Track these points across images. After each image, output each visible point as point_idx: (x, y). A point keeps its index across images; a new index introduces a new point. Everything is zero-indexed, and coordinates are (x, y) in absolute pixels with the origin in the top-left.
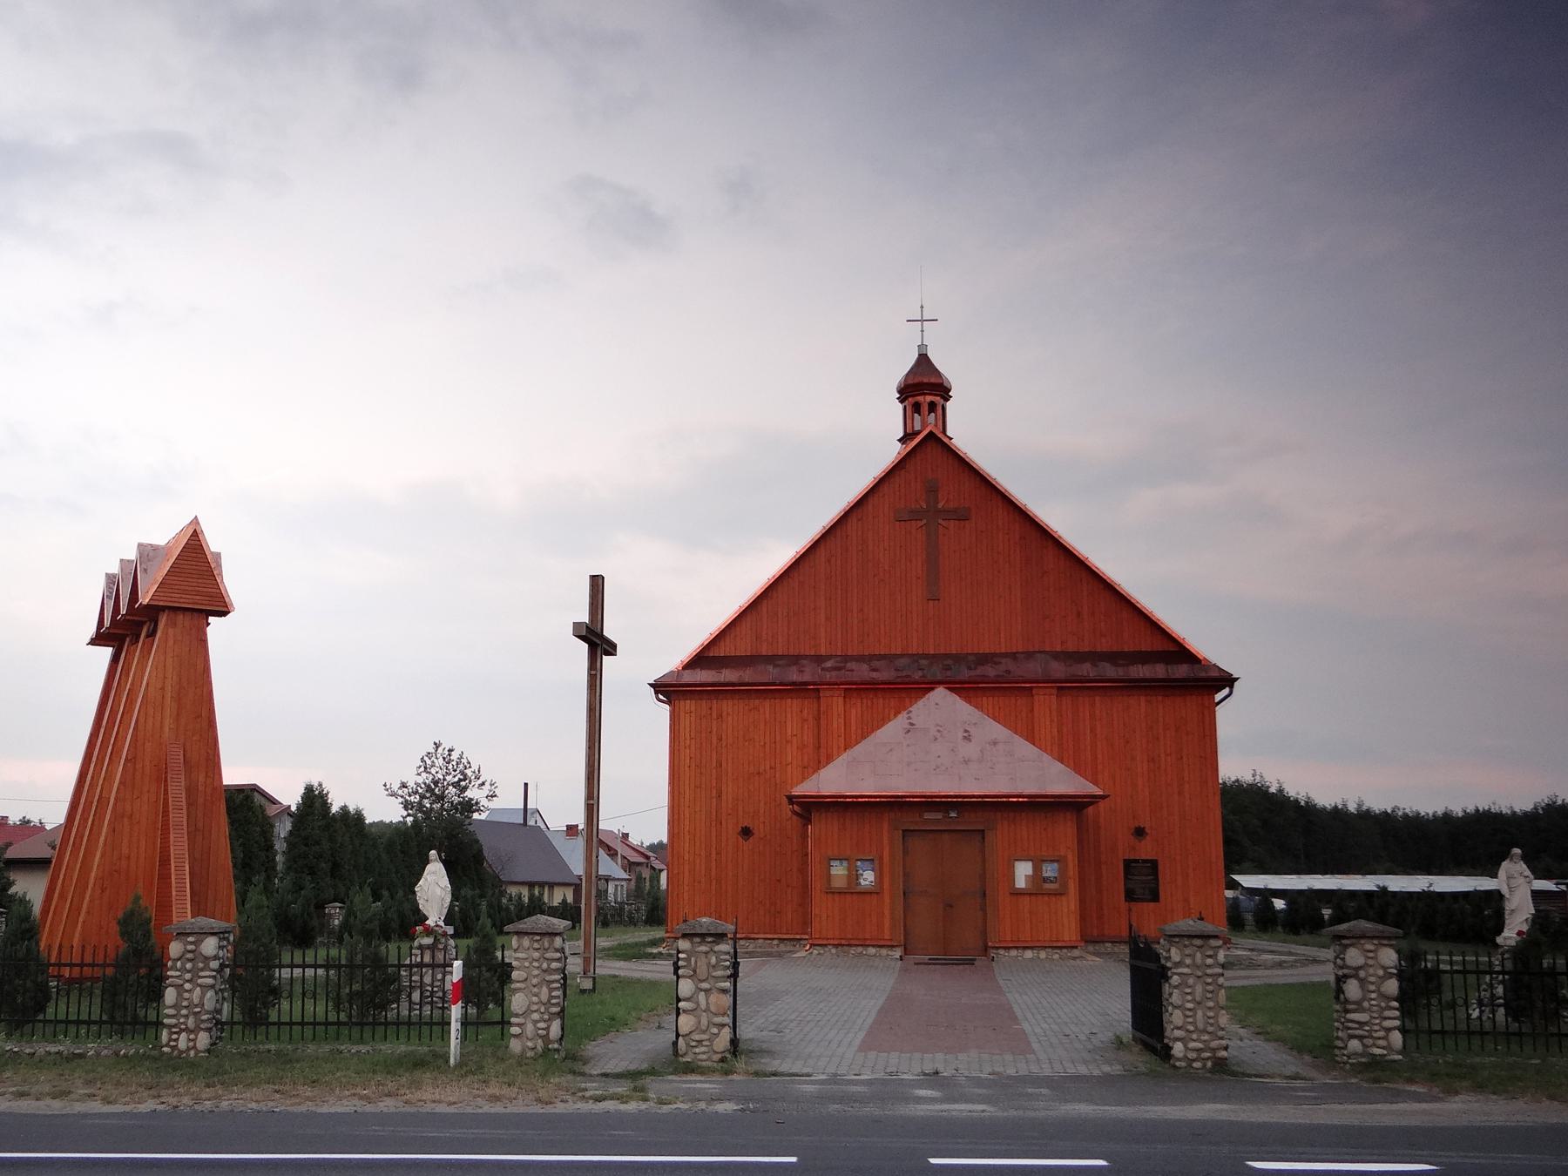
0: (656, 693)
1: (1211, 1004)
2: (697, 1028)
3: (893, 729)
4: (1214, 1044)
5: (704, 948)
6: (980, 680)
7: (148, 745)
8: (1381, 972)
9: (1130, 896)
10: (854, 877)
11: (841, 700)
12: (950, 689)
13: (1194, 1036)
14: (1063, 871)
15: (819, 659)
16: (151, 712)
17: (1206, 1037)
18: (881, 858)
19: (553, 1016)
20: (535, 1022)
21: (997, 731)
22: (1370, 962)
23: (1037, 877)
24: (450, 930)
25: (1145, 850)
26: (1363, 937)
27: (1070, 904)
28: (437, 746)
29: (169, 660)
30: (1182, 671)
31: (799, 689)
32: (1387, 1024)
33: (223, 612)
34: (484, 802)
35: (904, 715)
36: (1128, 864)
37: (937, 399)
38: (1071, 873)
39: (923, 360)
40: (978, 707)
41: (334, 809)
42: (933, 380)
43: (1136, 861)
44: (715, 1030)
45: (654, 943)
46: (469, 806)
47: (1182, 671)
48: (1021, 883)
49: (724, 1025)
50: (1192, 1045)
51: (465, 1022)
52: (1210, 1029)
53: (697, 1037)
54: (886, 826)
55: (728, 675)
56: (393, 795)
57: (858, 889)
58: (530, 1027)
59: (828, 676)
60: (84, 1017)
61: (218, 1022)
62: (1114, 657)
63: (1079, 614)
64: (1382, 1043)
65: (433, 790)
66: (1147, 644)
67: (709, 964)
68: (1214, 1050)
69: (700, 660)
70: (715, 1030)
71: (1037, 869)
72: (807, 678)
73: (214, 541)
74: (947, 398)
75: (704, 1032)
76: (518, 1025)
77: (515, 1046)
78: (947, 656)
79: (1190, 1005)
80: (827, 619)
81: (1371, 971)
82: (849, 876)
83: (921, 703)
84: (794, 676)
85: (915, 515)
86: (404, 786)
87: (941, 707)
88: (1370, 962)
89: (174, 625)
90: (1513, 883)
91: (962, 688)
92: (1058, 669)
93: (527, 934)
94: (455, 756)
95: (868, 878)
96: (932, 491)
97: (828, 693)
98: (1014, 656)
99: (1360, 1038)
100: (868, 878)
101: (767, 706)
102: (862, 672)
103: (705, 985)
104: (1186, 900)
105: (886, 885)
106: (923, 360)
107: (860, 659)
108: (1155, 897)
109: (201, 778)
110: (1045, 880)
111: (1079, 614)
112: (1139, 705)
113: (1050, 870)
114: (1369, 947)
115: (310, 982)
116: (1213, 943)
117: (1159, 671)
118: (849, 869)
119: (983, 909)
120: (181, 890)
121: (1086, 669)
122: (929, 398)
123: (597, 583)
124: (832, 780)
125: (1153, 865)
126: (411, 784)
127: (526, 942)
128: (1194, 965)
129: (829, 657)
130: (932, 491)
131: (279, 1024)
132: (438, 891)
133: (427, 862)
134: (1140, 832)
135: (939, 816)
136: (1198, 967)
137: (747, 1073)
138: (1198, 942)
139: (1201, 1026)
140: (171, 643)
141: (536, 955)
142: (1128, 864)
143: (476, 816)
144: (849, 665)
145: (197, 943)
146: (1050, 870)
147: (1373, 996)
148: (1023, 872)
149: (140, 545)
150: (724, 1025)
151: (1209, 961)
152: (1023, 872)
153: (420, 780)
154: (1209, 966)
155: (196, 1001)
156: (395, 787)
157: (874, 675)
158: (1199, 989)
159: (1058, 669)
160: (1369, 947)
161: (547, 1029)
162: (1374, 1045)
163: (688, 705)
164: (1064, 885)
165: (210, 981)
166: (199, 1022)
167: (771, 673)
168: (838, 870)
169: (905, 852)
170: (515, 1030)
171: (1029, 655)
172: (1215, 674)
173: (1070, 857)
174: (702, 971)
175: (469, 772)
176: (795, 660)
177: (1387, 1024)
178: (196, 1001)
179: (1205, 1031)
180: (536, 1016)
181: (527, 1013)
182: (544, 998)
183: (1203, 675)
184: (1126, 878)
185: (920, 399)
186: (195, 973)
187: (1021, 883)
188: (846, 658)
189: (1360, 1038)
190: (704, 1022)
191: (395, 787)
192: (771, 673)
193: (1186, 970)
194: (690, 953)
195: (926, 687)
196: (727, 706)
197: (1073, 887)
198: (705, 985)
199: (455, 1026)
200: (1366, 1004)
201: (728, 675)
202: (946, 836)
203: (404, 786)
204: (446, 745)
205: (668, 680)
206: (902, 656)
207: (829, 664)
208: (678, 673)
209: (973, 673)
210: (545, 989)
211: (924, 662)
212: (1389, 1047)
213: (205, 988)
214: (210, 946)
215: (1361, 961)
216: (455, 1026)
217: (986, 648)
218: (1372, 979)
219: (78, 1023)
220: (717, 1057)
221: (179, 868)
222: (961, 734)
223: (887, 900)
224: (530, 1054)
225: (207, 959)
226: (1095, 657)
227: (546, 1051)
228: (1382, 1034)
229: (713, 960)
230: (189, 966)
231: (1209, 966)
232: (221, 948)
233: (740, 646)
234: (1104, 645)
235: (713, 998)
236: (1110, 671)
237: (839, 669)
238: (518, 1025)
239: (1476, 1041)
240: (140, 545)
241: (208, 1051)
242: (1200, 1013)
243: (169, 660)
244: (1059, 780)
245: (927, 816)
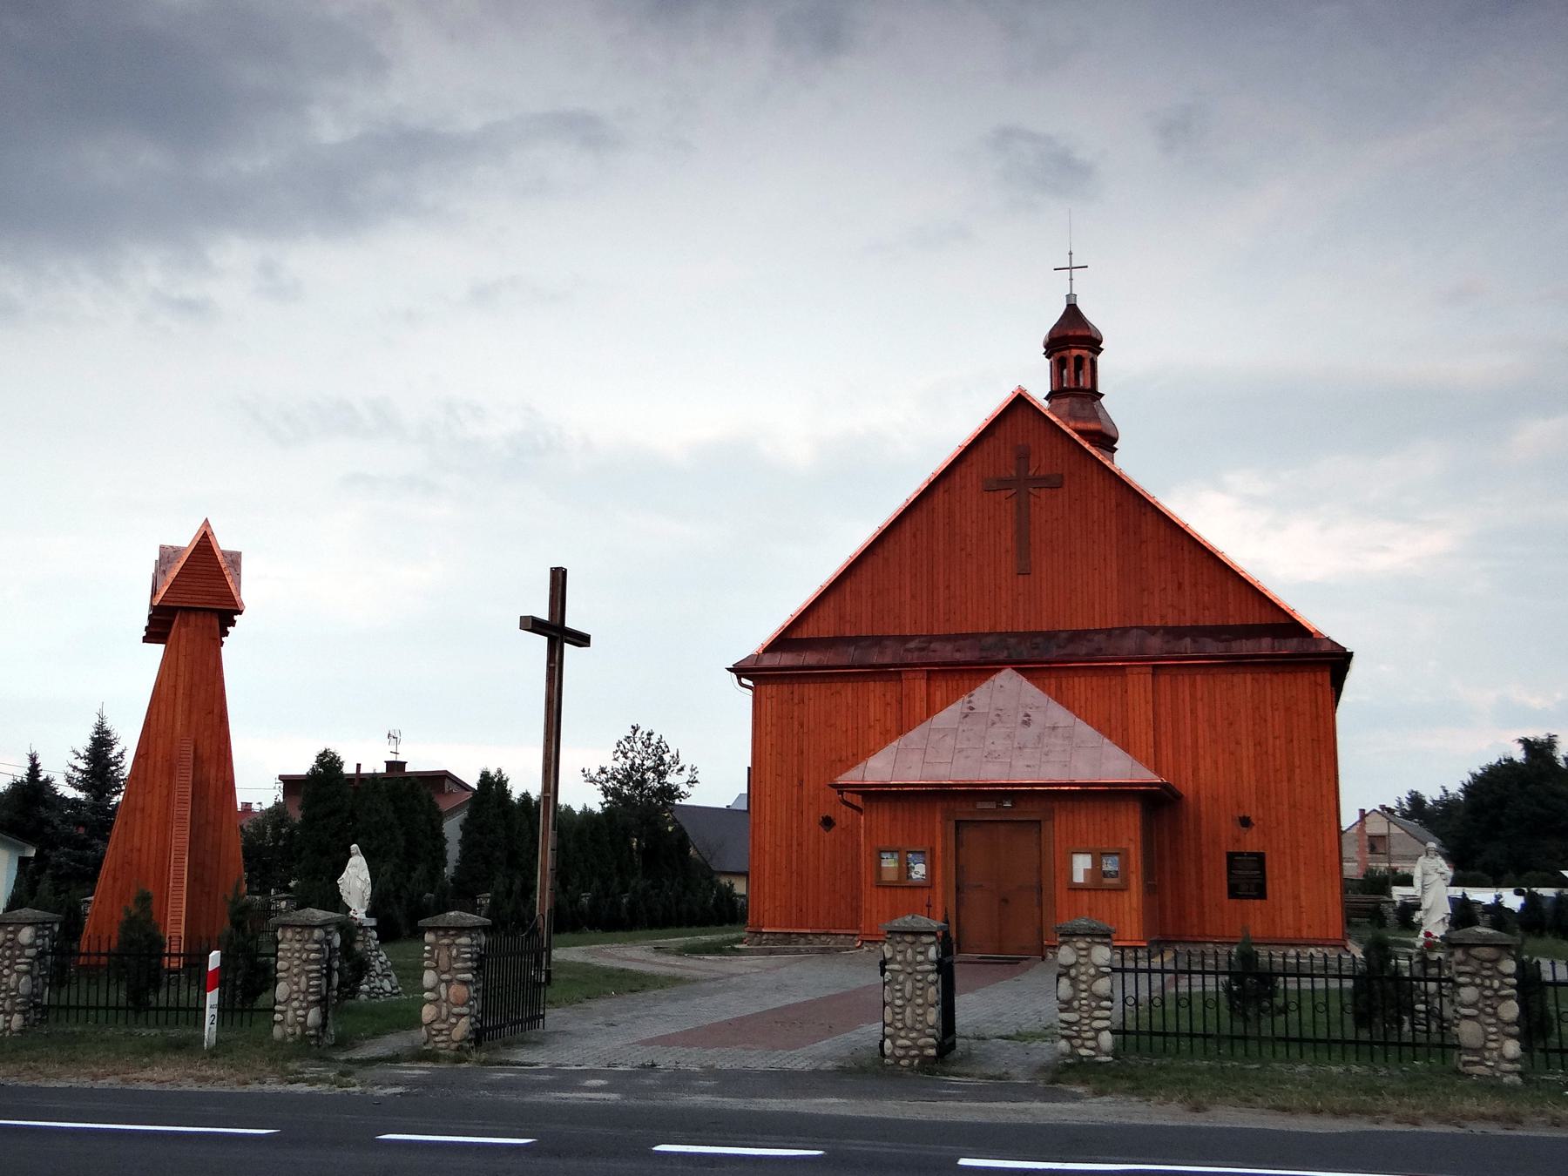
0: (739, 678)
1: (920, 1001)
2: (438, 1019)
3: (948, 716)
4: (921, 1042)
5: (445, 941)
6: (1051, 660)
7: (160, 741)
8: (1092, 971)
9: (1234, 892)
10: (906, 869)
11: (923, 683)
12: (1018, 670)
13: (902, 1034)
14: (1125, 865)
15: (905, 639)
16: (163, 708)
17: (914, 1035)
18: (932, 850)
19: (311, 1004)
20: (296, 1009)
21: (1059, 715)
22: (1082, 960)
23: (1096, 872)
24: (373, 922)
25: (1251, 842)
26: (1075, 935)
27: (1133, 899)
28: (635, 729)
29: (182, 659)
30: (1291, 646)
31: (880, 672)
32: (1097, 1024)
33: (240, 613)
34: (684, 788)
35: (966, 698)
36: (1231, 857)
37: (1085, 353)
38: (1133, 868)
39: (1072, 313)
40: (1043, 688)
41: (516, 795)
42: (1079, 333)
43: (1241, 854)
44: (453, 1020)
45: (741, 941)
46: (669, 792)
47: (1291, 646)
48: (1079, 878)
49: (463, 1015)
50: (900, 1042)
51: (222, 1008)
52: (919, 1026)
53: (436, 1026)
54: (938, 817)
55: (809, 658)
56: (593, 781)
57: (910, 883)
58: (290, 1014)
59: (909, 658)
60: (93, 1003)
61: (36, 1006)
62: (1215, 632)
63: (1180, 586)
64: (1089, 1043)
65: (632, 775)
66: (1254, 617)
67: (450, 957)
68: (921, 1048)
69: (783, 641)
70: (453, 1020)
71: (1096, 863)
72: (887, 660)
73: (224, 542)
74: (1098, 351)
75: (444, 1022)
76: (281, 1012)
77: (277, 1032)
78: (1040, 634)
79: (899, 1002)
80: (913, 597)
81: (1083, 969)
82: (900, 867)
83: (984, 686)
84: (875, 658)
85: (1004, 484)
86: (603, 771)
87: (1007, 689)
88: (1082, 960)
89: (187, 625)
90: (1429, 880)
91: (1030, 670)
92: (1155, 644)
93: (291, 926)
94: (654, 740)
95: (919, 870)
96: (1023, 456)
97: (911, 675)
98: (1109, 632)
99: (1068, 1038)
100: (919, 870)
101: (848, 691)
102: (946, 652)
103: (446, 977)
104: (1297, 897)
105: (938, 879)
106: (1072, 313)
107: (948, 638)
108: (1261, 893)
109: (213, 772)
110: (1105, 874)
111: (1180, 586)
112: (1244, 686)
113: (1110, 865)
114: (1082, 945)
115: (1321, 999)
116: (925, 939)
117: (1265, 646)
118: (900, 861)
119: (1040, 905)
120: (179, 880)
121: (1246, 647)
122: (1076, 352)
123: (559, 579)
124: (879, 769)
125: (1260, 858)
126: (609, 769)
127: (289, 934)
128: (904, 962)
129: (912, 638)
130: (1023, 456)
131: (158, 1009)
132: (359, 884)
133: (350, 856)
134: (1246, 822)
135: (993, 806)
136: (910, 964)
137: (478, 1062)
138: (909, 938)
139: (909, 1022)
140: (183, 642)
141: (298, 946)
142: (1231, 857)
143: (677, 802)
144: (933, 646)
145: (16, 932)
146: (1110, 865)
147: (1084, 995)
148: (1081, 865)
149: (162, 547)
150: (463, 1015)
151: (920, 958)
152: (1081, 865)
153: (618, 765)
154: (920, 963)
155: (12, 985)
156: (594, 772)
157: (958, 656)
158: (908, 986)
159: (1155, 644)
160: (1082, 945)
161: (305, 1016)
162: (1083, 1046)
163: (769, 689)
164: (1126, 880)
165: (24, 967)
166: (14, 1004)
167: (849, 655)
168: (889, 863)
169: (958, 844)
170: (278, 1017)
171: (1125, 631)
172: (1325, 648)
173: (1132, 849)
174: (444, 962)
175: (667, 757)
176: (878, 641)
177: (1097, 1024)
178: (12, 985)
179: (913, 1029)
180: (295, 1004)
181: (288, 1001)
182: (303, 986)
183: (1313, 649)
184: (1229, 872)
185: (1066, 353)
186: (13, 959)
187: (1079, 878)
188: (932, 638)
189: (1068, 1038)
190: (444, 1011)
191: (594, 772)
192: (849, 655)
193: (897, 967)
194: (434, 946)
195: (982, 669)
196: (809, 690)
197: (1136, 882)
198: (446, 977)
199: (210, 1012)
200: (1076, 1004)
201: (809, 658)
202: (1002, 827)
203: (603, 771)
204: (645, 729)
205: (749, 665)
206: (989, 634)
207: (912, 645)
208: (757, 657)
209: (1062, 652)
210: (304, 979)
211: (1012, 641)
212: (1097, 1049)
213: (21, 973)
214: (26, 935)
215: (1072, 959)
216: (210, 1012)
217: (1080, 624)
218: (1084, 978)
219: (88, 1008)
220: (454, 1046)
221: (179, 861)
222: (1021, 717)
223: (939, 890)
224: (290, 1040)
225: (23, 947)
226: (1197, 632)
227: (304, 1036)
228: (1090, 1034)
229: (454, 952)
230: (8, 953)
231: (920, 963)
232: (37, 937)
233: (823, 627)
234: (1207, 620)
235: (454, 988)
236: (1212, 647)
237: (922, 649)
238: (281, 1012)
239: (1184, 1043)
240: (162, 547)
241: (20, 1031)
242: (908, 1010)
243: (182, 659)
244: (1116, 766)
245: (980, 805)
